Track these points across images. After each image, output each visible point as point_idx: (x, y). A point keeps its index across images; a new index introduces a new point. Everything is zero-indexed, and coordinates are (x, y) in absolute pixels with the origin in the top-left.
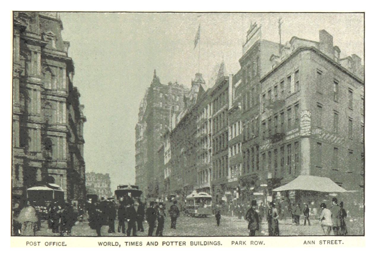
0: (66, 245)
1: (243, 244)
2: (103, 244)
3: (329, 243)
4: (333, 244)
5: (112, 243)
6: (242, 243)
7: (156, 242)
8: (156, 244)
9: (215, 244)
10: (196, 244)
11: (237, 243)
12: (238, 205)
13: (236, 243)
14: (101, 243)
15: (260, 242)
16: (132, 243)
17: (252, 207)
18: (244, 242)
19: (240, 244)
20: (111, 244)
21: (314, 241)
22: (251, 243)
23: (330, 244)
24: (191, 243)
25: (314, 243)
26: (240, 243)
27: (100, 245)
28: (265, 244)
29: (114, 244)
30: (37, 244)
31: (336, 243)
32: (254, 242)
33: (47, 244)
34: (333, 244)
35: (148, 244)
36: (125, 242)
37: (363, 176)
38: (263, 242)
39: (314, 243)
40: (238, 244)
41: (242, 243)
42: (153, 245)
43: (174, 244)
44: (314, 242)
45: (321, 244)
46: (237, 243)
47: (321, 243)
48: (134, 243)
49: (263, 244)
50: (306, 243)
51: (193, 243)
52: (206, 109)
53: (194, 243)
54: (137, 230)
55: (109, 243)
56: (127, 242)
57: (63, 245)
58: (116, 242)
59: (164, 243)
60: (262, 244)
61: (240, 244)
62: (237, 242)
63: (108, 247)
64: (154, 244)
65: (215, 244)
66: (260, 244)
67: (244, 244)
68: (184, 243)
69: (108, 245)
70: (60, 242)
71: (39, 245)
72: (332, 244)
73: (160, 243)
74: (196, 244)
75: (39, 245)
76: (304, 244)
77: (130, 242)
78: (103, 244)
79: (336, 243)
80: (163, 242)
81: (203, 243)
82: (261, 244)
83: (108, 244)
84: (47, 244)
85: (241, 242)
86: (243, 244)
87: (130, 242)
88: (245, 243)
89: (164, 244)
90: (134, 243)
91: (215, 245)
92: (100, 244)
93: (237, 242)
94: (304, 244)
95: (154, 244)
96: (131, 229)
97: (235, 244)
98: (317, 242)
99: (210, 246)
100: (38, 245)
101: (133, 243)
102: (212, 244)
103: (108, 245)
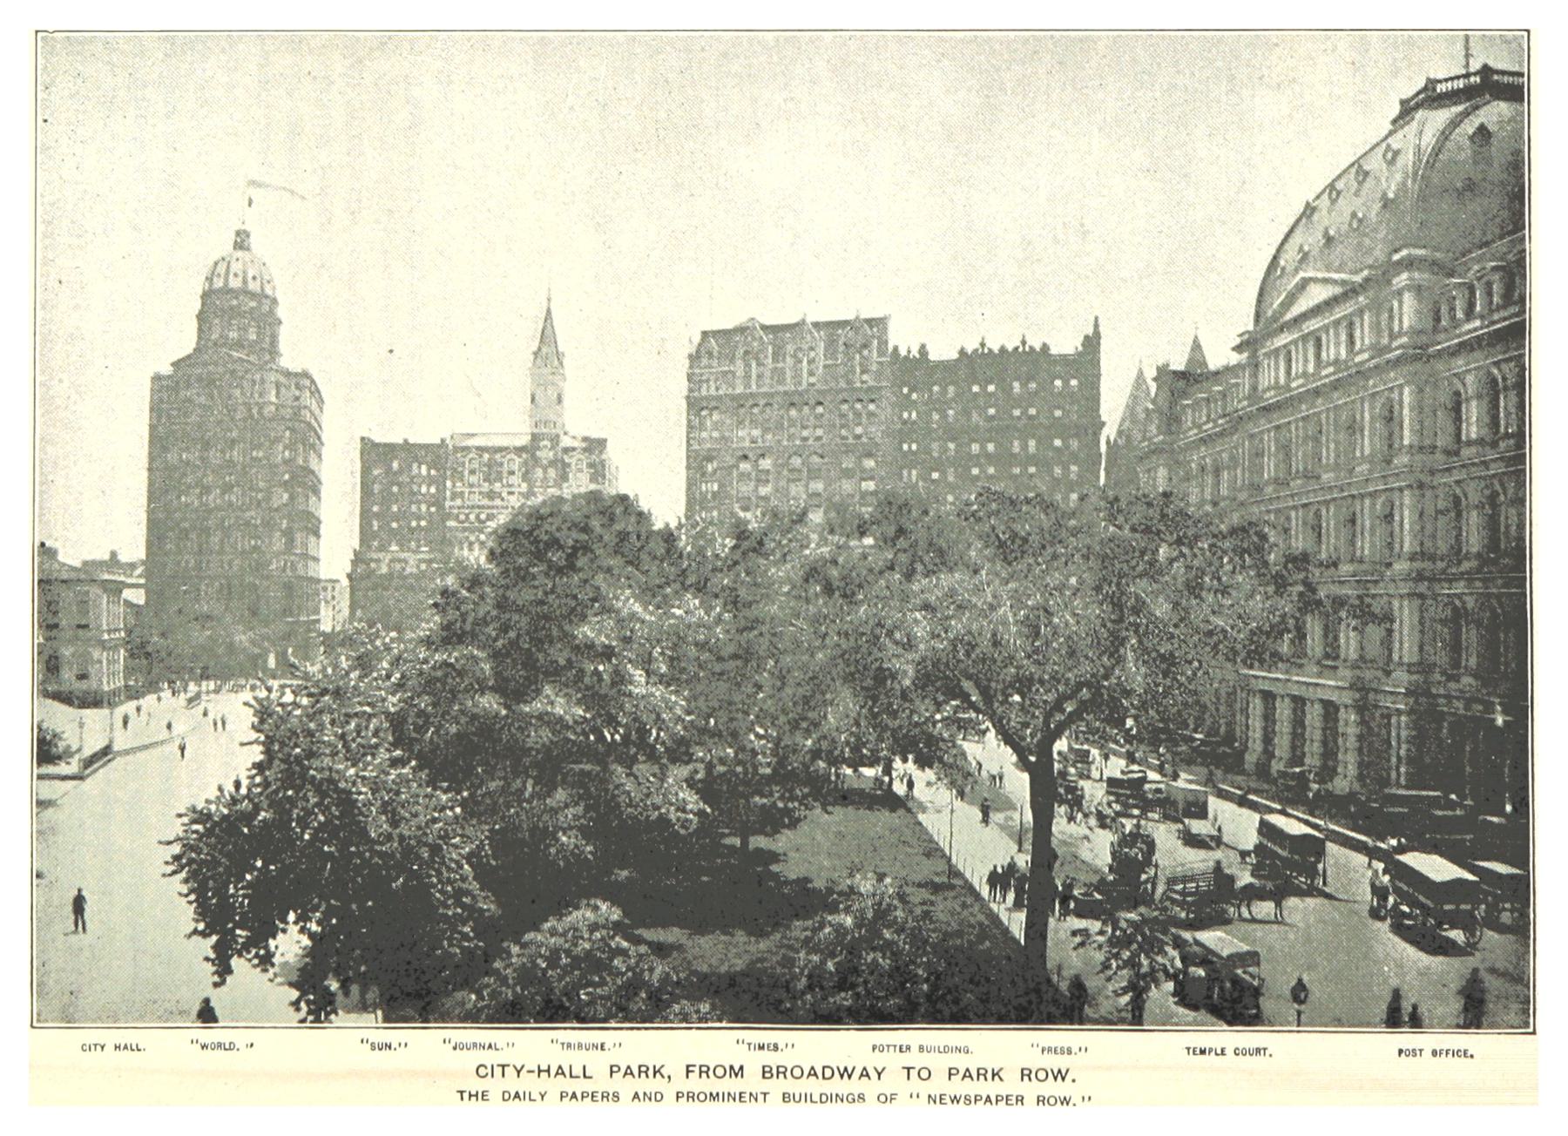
3: (704, 1075)
8: (482, 1071)
10: (797, 1098)
11: (574, 1096)
12: (296, 555)
14: (1064, 1072)
17: (1278, 904)
22: (1023, 1075)
24: (764, 1072)
27: (1059, 1078)
30: (761, 1097)
33: (507, 1096)
37: (1273, 918)
43: (892, 1049)
49: (1069, 1078)
51: (770, 1071)
52: (923, 777)
54: (1277, 820)
55: (781, 1070)
56: (462, 1092)
60: (1063, 1079)
66: (842, 1076)
67: (996, 1078)
74: (797, 1098)
76: (1092, 343)
78: (806, 1073)
80: (688, 1066)
81: (816, 1098)
82: (1059, 1078)
83: (778, 1073)
85: (1456, 1053)
88: (1001, 1074)
95: (820, 1075)
96: (1398, 861)
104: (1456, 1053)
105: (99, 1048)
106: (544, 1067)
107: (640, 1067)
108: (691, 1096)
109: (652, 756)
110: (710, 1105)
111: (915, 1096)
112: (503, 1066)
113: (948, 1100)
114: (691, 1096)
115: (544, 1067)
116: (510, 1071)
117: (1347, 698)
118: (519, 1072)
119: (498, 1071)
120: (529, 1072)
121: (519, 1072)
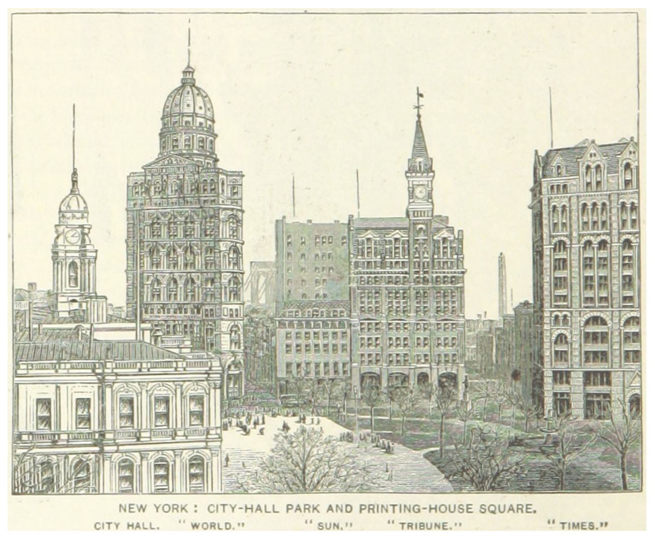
0: (535, 512)
1: (313, 512)
2: (161, 507)
3: (371, 511)
4: (134, 512)
5: (219, 524)
6: (179, 509)
7: (347, 506)
9: (417, 511)
10: (429, 527)
11: (298, 508)
13: (297, 509)
14: (144, 507)
15: (139, 506)
16: (574, 524)
18: (315, 506)
19: (518, 512)
20: (216, 527)
21: (120, 511)
23: (374, 512)
25: (121, 506)
26: (305, 509)
27: (141, 510)
28: (537, 512)
29: (222, 526)
31: (470, 510)
32: (456, 511)
34: (134, 512)
35: (330, 508)
36: (401, 523)
38: (146, 506)
39: (121, 506)
40: (514, 512)
41: (179, 509)
42: (125, 510)
44: (386, 507)
45: (461, 513)
46: (298, 508)
47: (321, 528)
48: (578, 524)
50: (332, 510)
53: (324, 526)
55: (175, 507)
57: (529, 510)
58: (226, 524)
59: (363, 507)
61: (520, 511)
62: (298, 506)
63: (210, 532)
64: (344, 510)
65: (417, 511)
66: (139, 510)
67: (183, 511)
68: (468, 509)
69: (173, 511)
70: (98, 523)
71: (224, 511)
72: (130, 512)
73: (476, 508)
74: (429, 527)
75: (224, 511)
76: (327, 511)
77: (401, 506)
78: (161, 507)
79: (470, 510)
80: (35, 284)
82: (141, 510)
83: (173, 509)
84: (98, 526)
85: (520, 508)
86: (313, 512)
87: (401, 506)
88: (186, 508)
89: (291, 509)
90: (578, 524)
91: (416, 512)
92: (195, 526)
93: (298, 506)
94: (327, 511)
95: (344, 510)
97: (295, 511)
98: (476, 508)
99: (382, 514)
100: (222, 511)
101: (576, 524)
102: (409, 511)
103: (173, 511)
104: (520, 508)
105: (113, 526)
106: (249, 506)
107: (518, 505)
108: (410, 526)
109: (102, 440)
110: (579, 532)
111: (458, 525)
112: (224, 505)
113: (136, 509)
114: (410, 526)
115: (433, 506)
116: (228, 508)
117: (383, 397)
118: (233, 509)
119: (221, 508)
120: (425, 508)
121: (233, 509)
